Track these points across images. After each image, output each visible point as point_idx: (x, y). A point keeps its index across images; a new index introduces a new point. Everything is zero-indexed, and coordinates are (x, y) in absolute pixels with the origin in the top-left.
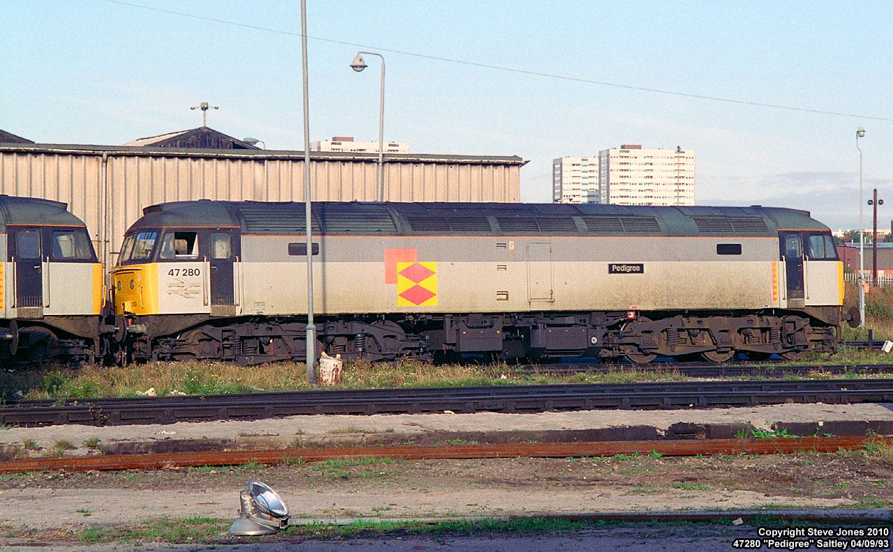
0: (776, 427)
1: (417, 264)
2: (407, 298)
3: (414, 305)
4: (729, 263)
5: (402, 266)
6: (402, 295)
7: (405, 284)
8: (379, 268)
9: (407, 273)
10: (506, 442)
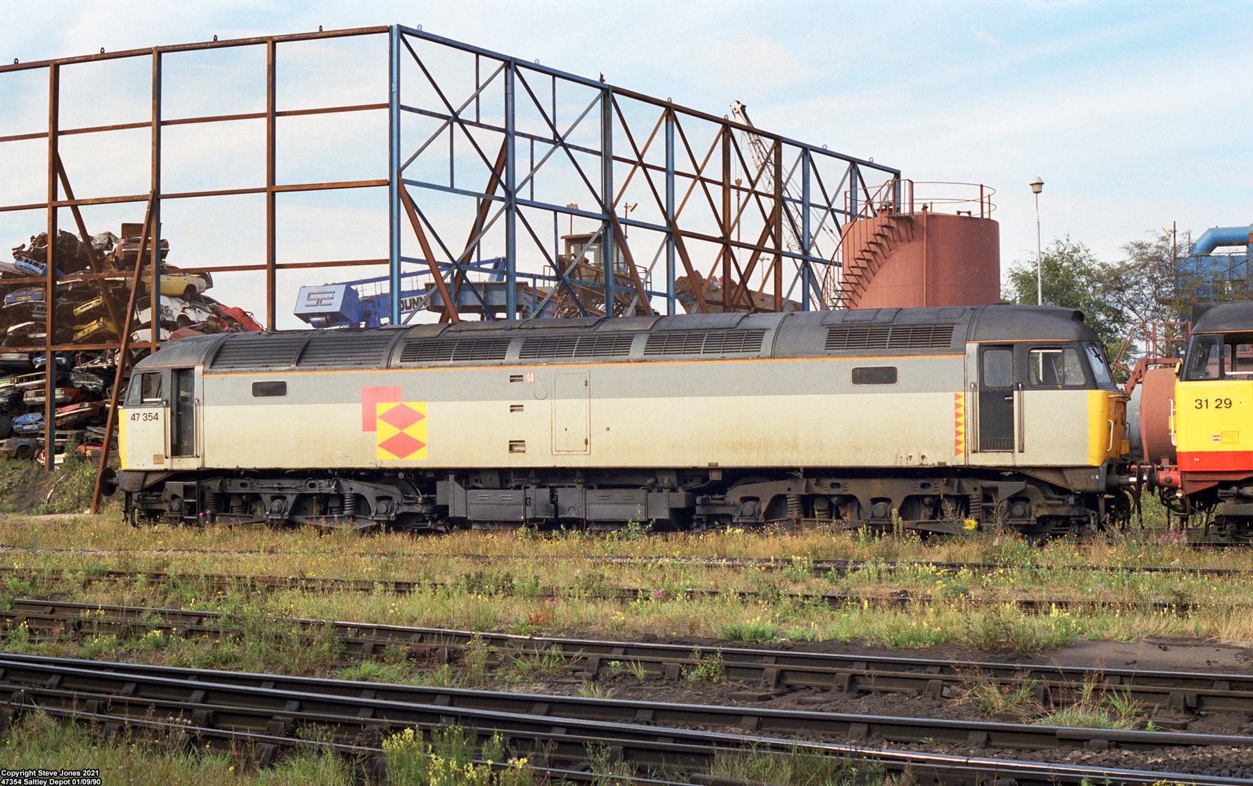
0: (435, 516)
1: (404, 406)
2: (389, 450)
3: (396, 458)
4: (876, 398)
5: (382, 408)
6: (382, 445)
7: (386, 431)
8: (353, 412)
9: (387, 417)
10: (742, 594)
